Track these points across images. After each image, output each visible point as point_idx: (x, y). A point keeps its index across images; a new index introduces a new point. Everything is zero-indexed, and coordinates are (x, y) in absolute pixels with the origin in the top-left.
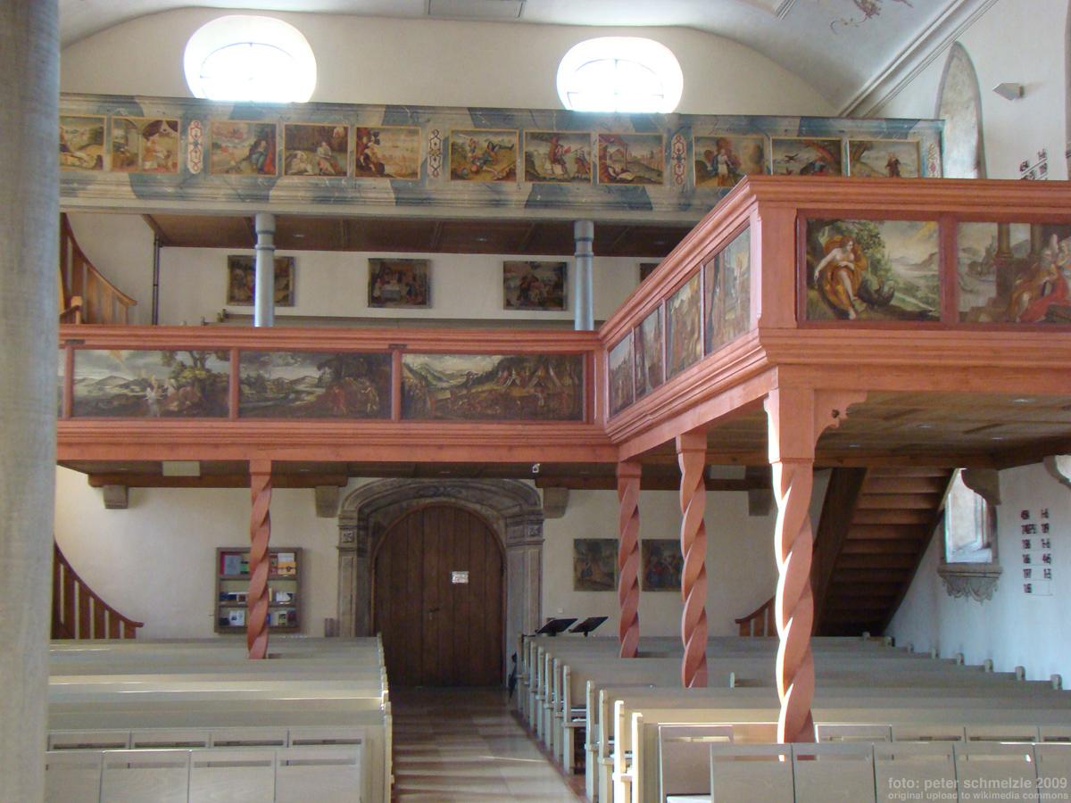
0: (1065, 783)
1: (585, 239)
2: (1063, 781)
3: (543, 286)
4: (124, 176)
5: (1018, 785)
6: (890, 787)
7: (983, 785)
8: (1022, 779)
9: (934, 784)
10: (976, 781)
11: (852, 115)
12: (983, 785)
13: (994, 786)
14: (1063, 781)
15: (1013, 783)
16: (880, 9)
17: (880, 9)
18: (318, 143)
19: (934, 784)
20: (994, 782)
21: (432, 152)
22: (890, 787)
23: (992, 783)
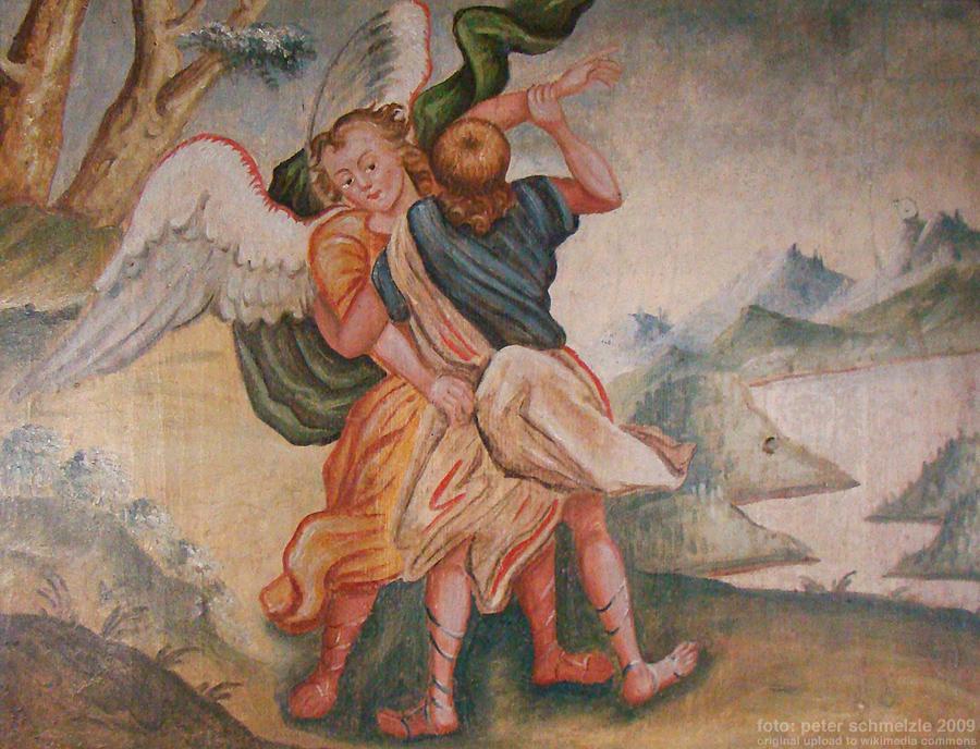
5: (916, 727)
6: (760, 730)
22: (760, 730)
23: (883, 726)
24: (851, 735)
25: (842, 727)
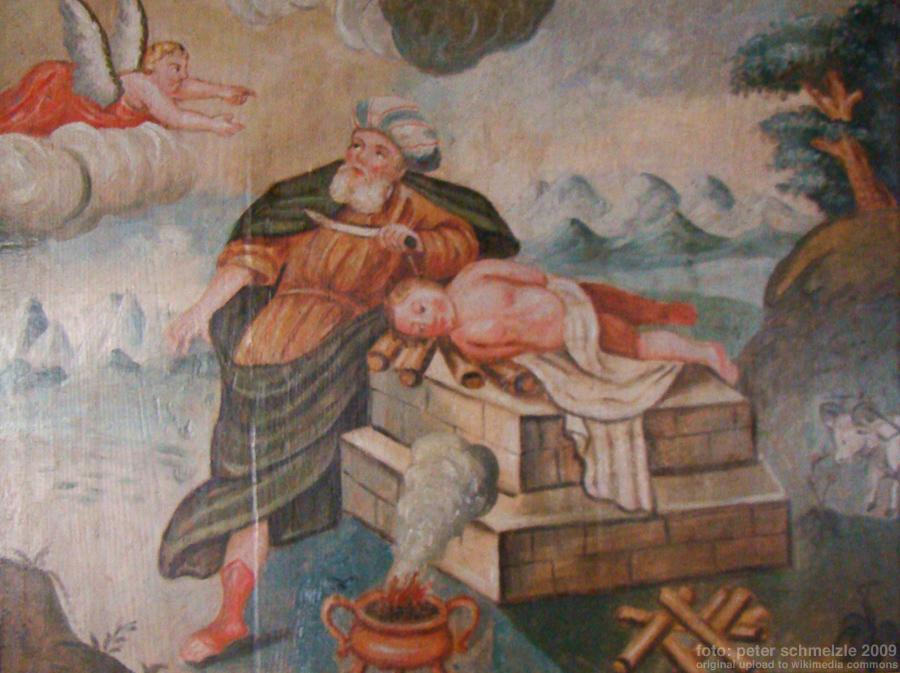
0: (895, 651)
1: (695, 280)
2: (892, 649)
3: (582, 324)
4: (251, 365)
5: (842, 652)
7: (817, 653)
8: (846, 646)
9: (824, 651)
10: (796, 649)
11: (310, 243)
12: (817, 653)
13: (805, 655)
14: (892, 649)
15: (836, 651)
16: (746, 96)
17: (746, 96)
18: (45, 374)
19: (824, 651)
20: (815, 649)
21: (457, 292)
23: (812, 651)
24: (784, 659)
25: (774, 651)
